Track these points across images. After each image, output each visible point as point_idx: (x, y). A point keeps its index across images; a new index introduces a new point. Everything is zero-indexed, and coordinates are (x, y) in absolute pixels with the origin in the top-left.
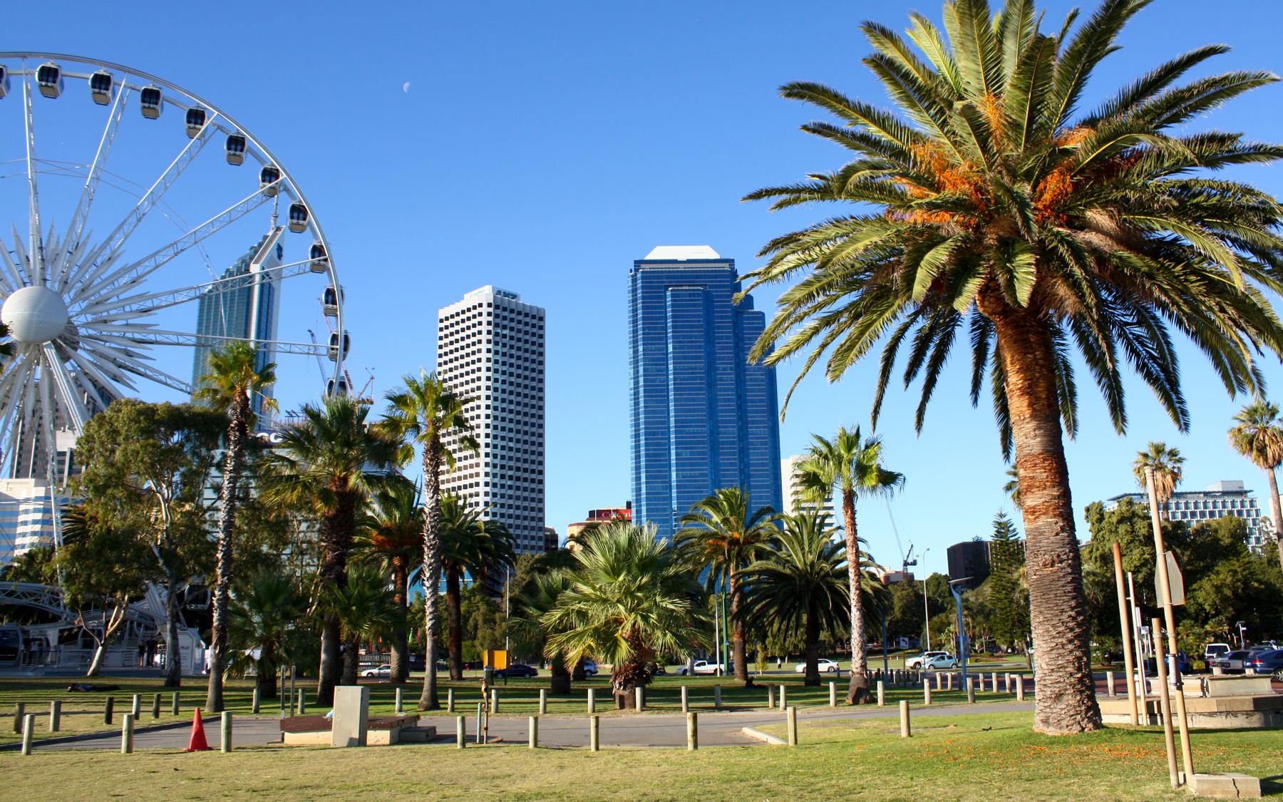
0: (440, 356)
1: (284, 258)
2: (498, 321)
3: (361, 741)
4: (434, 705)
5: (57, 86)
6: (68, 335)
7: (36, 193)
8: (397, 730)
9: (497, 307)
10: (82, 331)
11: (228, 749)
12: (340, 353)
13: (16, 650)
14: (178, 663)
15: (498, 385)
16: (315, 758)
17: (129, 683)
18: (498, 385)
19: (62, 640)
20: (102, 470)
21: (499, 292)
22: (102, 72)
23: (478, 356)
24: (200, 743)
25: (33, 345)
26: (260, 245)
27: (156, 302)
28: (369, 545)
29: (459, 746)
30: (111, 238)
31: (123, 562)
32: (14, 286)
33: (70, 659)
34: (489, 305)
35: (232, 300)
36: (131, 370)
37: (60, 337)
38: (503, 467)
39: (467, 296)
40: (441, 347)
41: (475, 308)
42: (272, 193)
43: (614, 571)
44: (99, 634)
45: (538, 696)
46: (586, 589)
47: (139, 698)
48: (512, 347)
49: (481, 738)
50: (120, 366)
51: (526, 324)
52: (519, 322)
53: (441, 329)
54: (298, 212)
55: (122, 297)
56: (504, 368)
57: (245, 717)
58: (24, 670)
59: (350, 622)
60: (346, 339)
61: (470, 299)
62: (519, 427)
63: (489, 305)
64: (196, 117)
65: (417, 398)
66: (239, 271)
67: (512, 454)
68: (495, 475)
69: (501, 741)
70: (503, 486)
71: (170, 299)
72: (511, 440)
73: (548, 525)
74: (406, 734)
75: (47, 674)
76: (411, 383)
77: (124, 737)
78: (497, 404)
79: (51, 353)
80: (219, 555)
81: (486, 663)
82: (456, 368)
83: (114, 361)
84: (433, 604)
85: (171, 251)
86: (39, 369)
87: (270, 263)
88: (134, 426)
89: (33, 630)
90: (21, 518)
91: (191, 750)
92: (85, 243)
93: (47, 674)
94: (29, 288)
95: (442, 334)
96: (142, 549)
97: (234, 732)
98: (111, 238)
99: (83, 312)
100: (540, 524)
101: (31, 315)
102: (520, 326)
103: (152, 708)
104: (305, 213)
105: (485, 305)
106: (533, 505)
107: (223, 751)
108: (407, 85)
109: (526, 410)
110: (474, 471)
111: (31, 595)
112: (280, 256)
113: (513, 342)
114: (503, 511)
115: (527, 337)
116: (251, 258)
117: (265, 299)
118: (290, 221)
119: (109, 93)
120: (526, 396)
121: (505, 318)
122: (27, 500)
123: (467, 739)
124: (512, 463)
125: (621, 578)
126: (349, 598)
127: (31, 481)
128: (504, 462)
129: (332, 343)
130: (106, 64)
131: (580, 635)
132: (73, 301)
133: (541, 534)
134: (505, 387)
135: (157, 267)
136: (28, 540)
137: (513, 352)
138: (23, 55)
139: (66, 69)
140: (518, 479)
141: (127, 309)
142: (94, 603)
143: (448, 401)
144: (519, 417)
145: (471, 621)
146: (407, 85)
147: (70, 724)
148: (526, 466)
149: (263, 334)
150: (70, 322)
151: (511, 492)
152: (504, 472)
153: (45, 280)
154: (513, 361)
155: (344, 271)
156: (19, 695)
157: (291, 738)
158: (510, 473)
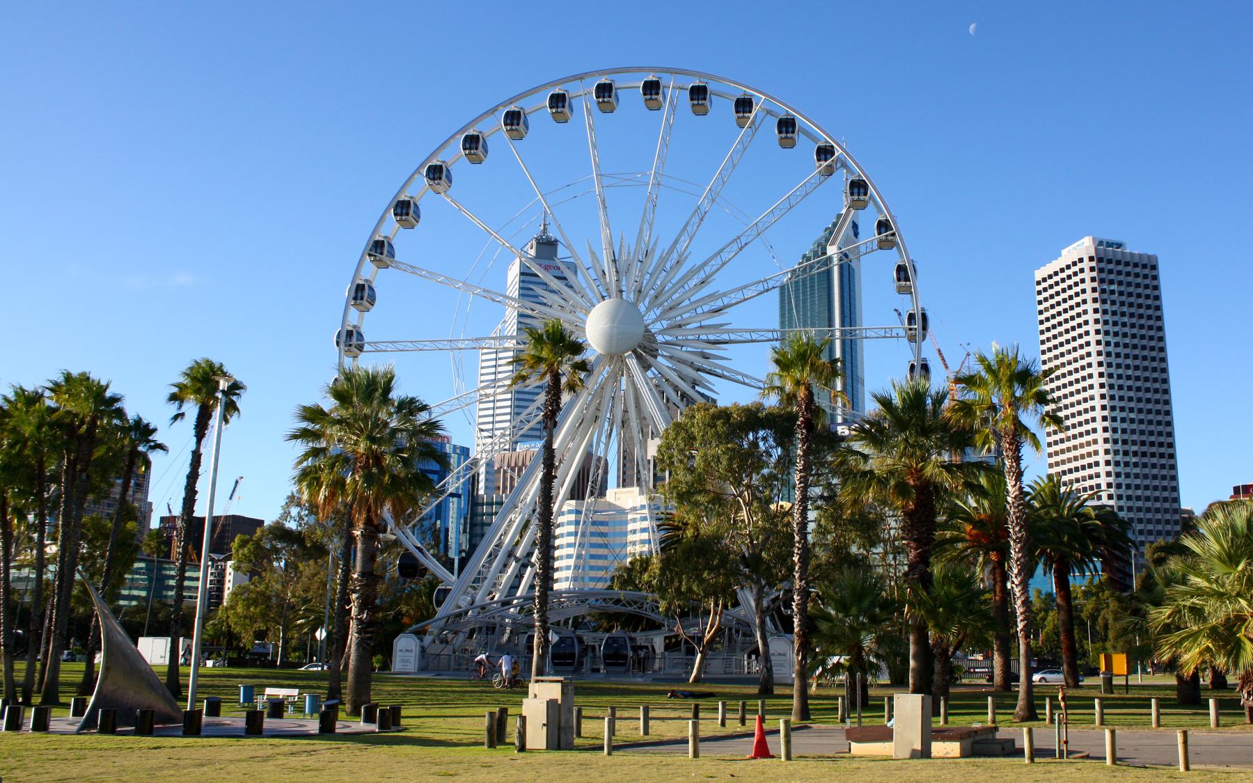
0: (1041, 322)
1: (860, 236)
2: (1103, 275)
3: (925, 753)
4: (1031, 715)
5: (613, 100)
6: (647, 344)
7: (605, 207)
8: (969, 741)
9: (1100, 260)
10: (660, 338)
11: (788, 757)
12: (919, 332)
13: (626, 656)
14: (770, 670)
15: (1110, 349)
16: (869, 769)
17: (727, 690)
18: (1110, 349)
19: (667, 648)
20: (682, 475)
21: (1101, 243)
22: (651, 78)
23: (1084, 318)
24: (762, 751)
25: (614, 356)
26: (835, 225)
27: (726, 301)
28: (962, 540)
29: (1027, 761)
30: (676, 242)
31: (711, 569)
32: (594, 300)
33: (674, 666)
34: (1091, 259)
35: (812, 287)
36: (709, 373)
37: (640, 346)
38: (1125, 442)
39: (1064, 252)
40: (1041, 312)
41: (1074, 264)
42: (829, 171)
43: (1231, 559)
44: (700, 639)
45: (1150, 707)
46: (1202, 583)
47: (724, 705)
48: (1122, 304)
49: (1061, 752)
50: (698, 370)
51: (1137, 275)
52: (1128, 274)
53: (1039, 293)
54: (858, 187)
55: (693, 299)
56: (1116, 329)
57: (830, 726)
58: (634, 675)
59: (937, 625)
60: (924, 317)
61: (1069, 254)
62: (1140, 394)
63: (1091, 259)
64: (744, 105)
65: (988, 377)
66: (816, 255)
67: (1134, 426)
68: (1116, 452)
69: (1087, 757)
70: (1127, 464)
71: (740, 296)
72: (1131, 410)
73: (1184, 505)
74: (981, 746)
75: (654, 680)
76: (982, 360)
77: (691, 742)
78: (1112, 370)
79: (632, 363)
80: (796, 559)
81: (1103, 668)
82: (1061, 334)
83: (692, 365)
84: (1023, 602)
85: (735, 247)
86: (624, 379)
87: (846, 242)
88: (711, 432)
89: (640, 637)
90: (630, 527)
91: (754, 758)
92: (653, 249)
93: (654, 680)
94: (607, 301)
95: (1040, 298)
96: (724, 555)
97: (793, 740)
98: (676, 242)
99: (658, 319)
100: (1175, 506)
101: (612, 328)
102: (1130, 279)
103: (738, 716)
104: (865, 187)
105: (1086, 259)
106: (1165, 483)
107: (783, 759)
108: (972, 27)
109: (1147, 374)
110: (1091, 449)
111: (636, 603)
112: (856, 234)
113: (1123, 298)
114: (1130, 492)
115: (1140, 290)
116: (827, 240)
117: (846, 281)
118: (850, 198)
119: (660, 97)
120: (1145, 358)
121: (1110, 272)
122: (634, 509)
123: (1036, 753)
124: (1135, 437)
125: (1240, 568)
126: (935, 599)
127: (636, 489)
128: (1126, 437)
129: (910, 323)
130: (652, 69)
131: (1194, 636)
132: (649, 309)
133: (1177, 517)
134: (1118, 350)
135: (724, 264)
136: (638, 549)
137: (1125, 309)
138: (581, 77)
139: (619, 81)
140: (1144, 454)
141: (699, 311)
142: (691, 612)
143: (1024, 377)
144: (1139, 384)
145: (1100, 620)
146: (972, 27)
147: (660, 729)
148: (1152, 439)
149: (847, 319)
150: (647, 331)
151: (1136, 470)
152: (1126, 447)
153: (621, 291)
154: (1126, 319)
155: (914, 246)
156: (625, 700)
157: (857, 748)
158: (1134, 448)
